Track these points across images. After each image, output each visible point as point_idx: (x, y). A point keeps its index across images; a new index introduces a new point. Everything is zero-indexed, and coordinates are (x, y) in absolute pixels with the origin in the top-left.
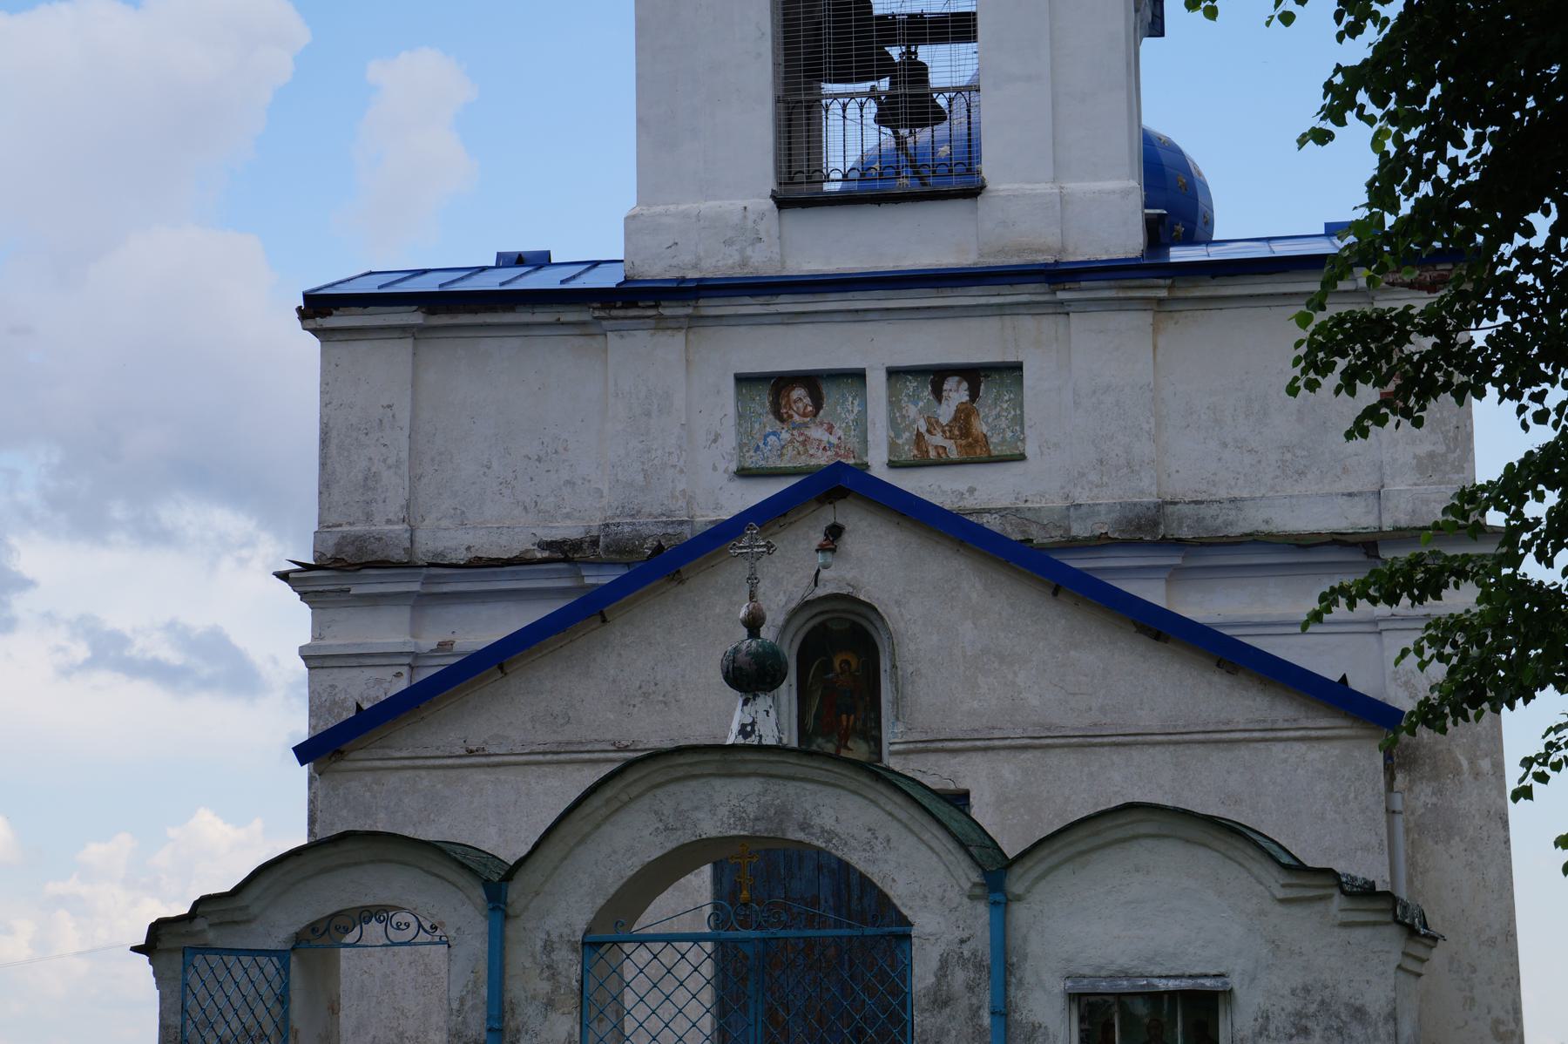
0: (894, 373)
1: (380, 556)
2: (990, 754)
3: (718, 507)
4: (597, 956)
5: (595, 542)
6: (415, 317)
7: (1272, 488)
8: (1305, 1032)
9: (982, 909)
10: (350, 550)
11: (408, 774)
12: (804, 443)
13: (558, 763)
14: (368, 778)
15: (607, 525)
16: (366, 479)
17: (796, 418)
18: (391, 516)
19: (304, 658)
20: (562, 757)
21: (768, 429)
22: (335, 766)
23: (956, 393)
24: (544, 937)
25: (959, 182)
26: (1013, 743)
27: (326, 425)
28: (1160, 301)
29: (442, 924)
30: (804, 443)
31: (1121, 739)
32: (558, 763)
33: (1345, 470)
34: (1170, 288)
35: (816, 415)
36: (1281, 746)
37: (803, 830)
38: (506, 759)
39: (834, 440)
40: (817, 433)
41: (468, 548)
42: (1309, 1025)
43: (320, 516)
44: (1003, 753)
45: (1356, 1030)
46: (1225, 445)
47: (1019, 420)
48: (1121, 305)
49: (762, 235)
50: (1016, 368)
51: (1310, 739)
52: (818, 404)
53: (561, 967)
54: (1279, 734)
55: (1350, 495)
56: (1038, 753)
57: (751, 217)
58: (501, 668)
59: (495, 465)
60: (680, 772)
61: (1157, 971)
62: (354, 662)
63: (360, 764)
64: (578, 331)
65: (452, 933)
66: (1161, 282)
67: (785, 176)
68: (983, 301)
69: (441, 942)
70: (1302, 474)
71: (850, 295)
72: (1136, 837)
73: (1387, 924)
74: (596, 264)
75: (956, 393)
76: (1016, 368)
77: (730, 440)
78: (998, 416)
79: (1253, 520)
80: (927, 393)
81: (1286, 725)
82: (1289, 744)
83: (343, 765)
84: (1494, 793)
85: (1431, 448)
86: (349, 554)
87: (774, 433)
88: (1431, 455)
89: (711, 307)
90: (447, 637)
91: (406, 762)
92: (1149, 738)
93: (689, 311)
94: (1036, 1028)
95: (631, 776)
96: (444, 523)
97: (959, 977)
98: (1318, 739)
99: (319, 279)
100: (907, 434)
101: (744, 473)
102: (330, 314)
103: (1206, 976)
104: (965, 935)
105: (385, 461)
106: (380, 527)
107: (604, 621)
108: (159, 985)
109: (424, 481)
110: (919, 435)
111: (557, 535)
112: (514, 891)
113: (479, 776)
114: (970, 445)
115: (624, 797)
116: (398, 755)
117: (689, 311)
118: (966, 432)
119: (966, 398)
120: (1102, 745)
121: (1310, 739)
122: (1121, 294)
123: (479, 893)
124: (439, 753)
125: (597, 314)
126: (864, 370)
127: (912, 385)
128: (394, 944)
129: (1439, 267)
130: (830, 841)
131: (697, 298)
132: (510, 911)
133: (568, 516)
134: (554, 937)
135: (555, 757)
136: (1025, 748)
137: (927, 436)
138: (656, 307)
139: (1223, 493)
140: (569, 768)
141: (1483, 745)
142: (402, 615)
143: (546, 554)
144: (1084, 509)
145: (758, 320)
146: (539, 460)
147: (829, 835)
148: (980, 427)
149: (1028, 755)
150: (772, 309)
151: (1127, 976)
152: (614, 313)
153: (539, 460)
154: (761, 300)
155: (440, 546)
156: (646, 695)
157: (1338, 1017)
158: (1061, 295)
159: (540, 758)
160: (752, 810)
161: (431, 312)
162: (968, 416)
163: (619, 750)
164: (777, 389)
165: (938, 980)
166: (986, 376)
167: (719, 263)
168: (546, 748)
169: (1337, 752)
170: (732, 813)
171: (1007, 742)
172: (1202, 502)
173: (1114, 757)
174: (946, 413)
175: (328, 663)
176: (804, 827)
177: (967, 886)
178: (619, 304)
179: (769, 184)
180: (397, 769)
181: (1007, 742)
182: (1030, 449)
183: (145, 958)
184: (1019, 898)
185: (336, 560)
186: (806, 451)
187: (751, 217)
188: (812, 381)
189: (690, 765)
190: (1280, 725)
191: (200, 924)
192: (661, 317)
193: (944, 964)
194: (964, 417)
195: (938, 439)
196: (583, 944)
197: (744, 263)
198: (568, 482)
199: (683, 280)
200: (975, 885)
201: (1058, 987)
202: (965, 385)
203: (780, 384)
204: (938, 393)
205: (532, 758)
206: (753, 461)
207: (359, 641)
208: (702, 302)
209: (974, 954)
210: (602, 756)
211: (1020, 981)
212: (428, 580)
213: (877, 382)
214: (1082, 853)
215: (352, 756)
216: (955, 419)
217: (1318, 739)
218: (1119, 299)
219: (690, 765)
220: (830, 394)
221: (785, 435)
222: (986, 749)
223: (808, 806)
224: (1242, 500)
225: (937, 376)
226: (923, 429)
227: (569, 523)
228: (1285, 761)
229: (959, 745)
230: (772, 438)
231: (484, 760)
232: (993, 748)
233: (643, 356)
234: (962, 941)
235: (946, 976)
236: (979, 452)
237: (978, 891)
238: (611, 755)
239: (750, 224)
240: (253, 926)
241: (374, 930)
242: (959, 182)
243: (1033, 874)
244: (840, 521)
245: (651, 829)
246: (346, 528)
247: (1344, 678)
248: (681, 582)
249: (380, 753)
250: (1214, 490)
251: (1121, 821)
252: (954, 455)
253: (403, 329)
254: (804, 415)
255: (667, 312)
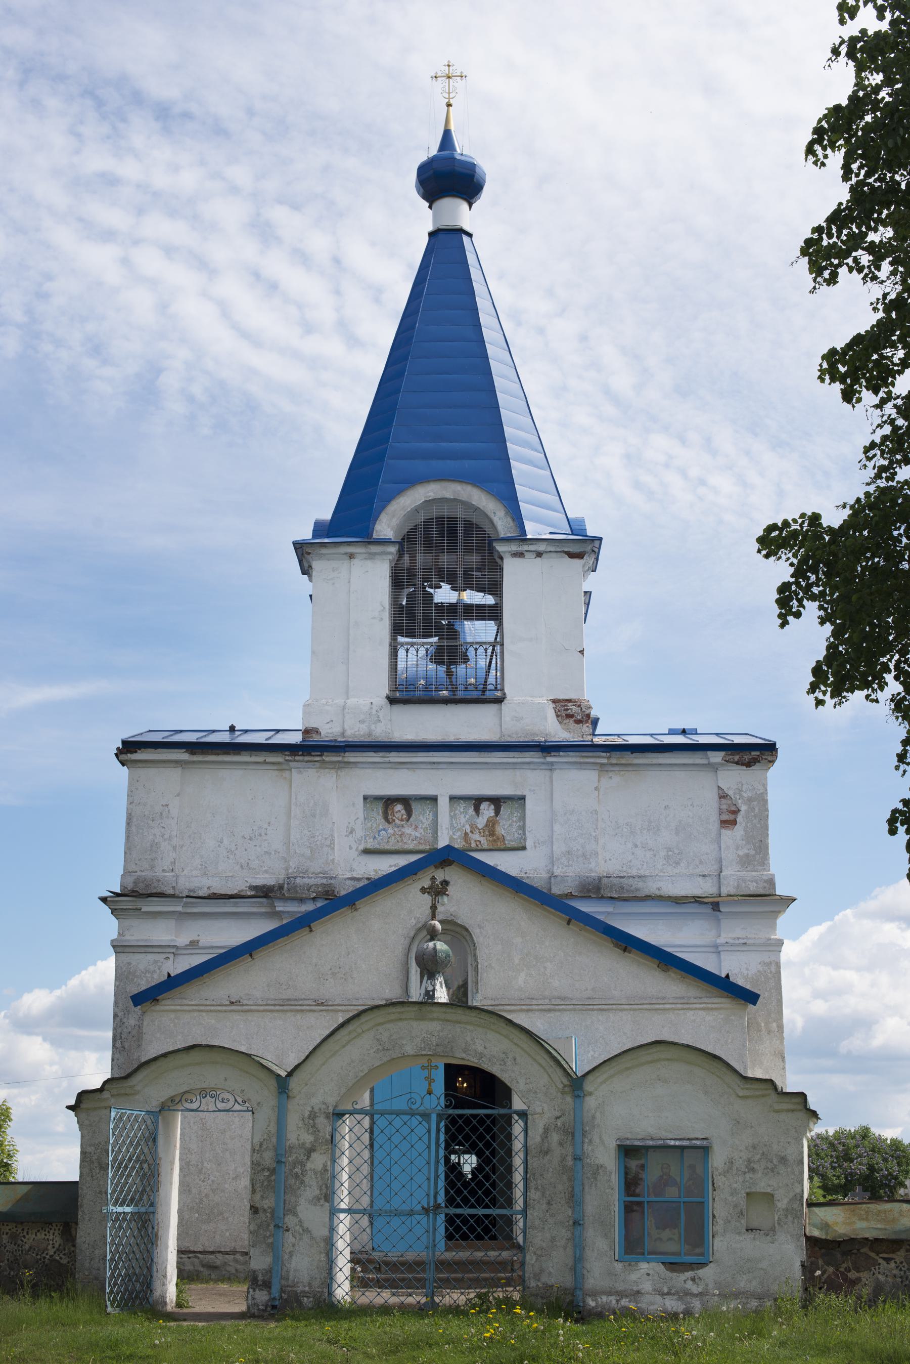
0: (452, 799)
1: (159, 891)
2: (530, 1013)
3: (352, 870)
4: (341, 1121)
5: (281, 887)
6: (183, 755)
7: (662, 871)
8: (753, 1170)
9: (569, 1099)
10: (141, 885)
11: (196, 1014)
12: (401, 836)
13: (282, 1011)
14: (172, 1016)
15: (289, 878)
16: (152, 846)
17: (397, 821)
18: (165, 868)
19: (114, 947)
20: (285, 1008)
21: (381, 827)
22: (153, 1008)
23: (487, 811)
24: (310, 1109)
25: (488, 696)
26: (543, 1007)
27: (130, 814)
28: (602, 765)
29: (249, 1100)
30: (401, 836)
31: (604, 1007)
32: (282, 1011)
33: (701, 862)
34: (609, 758)
35: (408, 820)
36: (692, 1012)
37: (465, 1052)
38: (253, 1008)
39: (418, 834)
40: (408, 830)
41: (209, 888)
42: (755, 1166)
43: (124, 866)
44: (537, 1013)
45: (782, 1169)
46: (636, 846)
47: (523, 828)
48: (581, 765)
49: (381, 718)
50: (523, 798)
51: (708, 1009)
52: (409, 813)
53: (320, 1126)
54: (691, 1006)
55: (704, 876)
56: (558, 1013)
57: (375, 708)
58: (251, 955)
59: (225, 841)
60: (393, 1017)
61: (671, 1136)
62: (143, 950)
63: (168, 1008)
64: (275, 768)
65: (255, 1106)
66: (604, 754)
67: (393, 687)
68: (520, 760)
69: (249, 1111)
70: (678, 863)
71: (431, 754)
72: (659, 1060)
73: (800, 1110)
74: (214, 731)
75: (487, 811)
76: (523, 798)
77: (359, 833)
78: (511, 825)
79: (651, 888)
80: (471, 811)
81: (695, 1001)
82: (696, 1012)
83: (158, 1008)
84: (778, 1042)
85: (747, 852)
86: (141, 888)
87: (384, 830)
88: (747, 855)
89: (351, 757)
90: (196, 938)
91: (195, 1008)
92: (620, 1007)
93: (340, 759)
94: (599, 1167)
95: (363, 1018)
96: (194, 873)
97: (555, 1137)
98: (712, 1009)
99: (130, 732)
100: (459, 833)
101: (367, 852)
102: (136, 752)
103: (697, 1139)
104: (559, 1114)
105: (163, 836)
106: (159, 873)
107: (311, 931)
108: (81, 1129)
109: (184, 848)
110: (466, 834)
111: (259, 882)
112: (293, 1083)
113: (236, 1017)
114: (495, 841)
115: (360, 1031)
116: (190, 1003)
117: (340, 759)
118: (492, 833)
119: (493, 814)
120: (593, 1010)
121: (708, 1009)
122: (582, 760)
123: (273, 1083)
124: (214, 1003)
125: (287, 758)
126: (437, 796)
127: (462, 806)
128: (220, 1111)
129: (753, 753)
130: (480, 1059)
131: (345, 752)
132: (290, 1094)
133: (266, 872)
134: (316, 1109)
135: (281, 1008)
136: (550, 1010)
137: (470, 834)
138: (321, 755)
139: (634, 872)
140: (289, 1014)
141: (773, 1015)
142: (171, 923)
143: (253, 893)
144: (559, 879)
145: (379, 765)
146: (251, 839)
147: (481, 1056)
148: (500, 830)
149: (552, 1014)
150: (387, 760)
151: (652, 1139)
152: (297, 758)
153: (251, 839)
154: (381, 754)
155: (192, 886)
156: (334, 974)
157: (771, 1162)
158: (549, 759)
159: (272, 1008)
160: (434, 1040)
161: (193, 753)
162: (494, 825)
163: (318, 1005)
164: (387, 804)
165: (543, 1140)
166: (504, 802)
167: (355, 731)
168: (276, 1002)
169: (722, 1016)
170: (423, 1040)
171: (540, 1007)
172: (623, 877)
173: (600, 1017)
174: (481, 822)
175: (127, 950)
176: (465, 1051)
177: (561, 1086)
178: (300, 753)
179: (386, 691)
180: (189, 1011)
181: (540, 1007)
182: (529, 844)
183: (72, 1113)
184: (590, 1094)
185: (133, 891)
186: (402, 840)
187: (375, 708)
188: (406, 801)
189: (400, 1013)
190: (692, 1000)
191: (106, 1095)
192: (323, 762)
193: (546, 1131)
194: (491, 825)
195: (476, 836)
196: (334, 1114)
197: (370, 735)
198: (266, 853)
199: (336, 741)
200: (565, 1086)
201: (613, 1144)
202: (492, 807)
203: (389, 802)
204: (477, 810)
205: (267, 1007)
206: (371, 844)
207: (145, 938)
208: (347, 754)
209: (564, 1125)
210: (308, 1008)
211: (590, 1141)
212: (186, 905)
213: (443, 803)
214: (627, 1069)
215: (163, 1002)
216: (486, 826)
217: (712, 1009)
218: (581, 763)
219: (400, 1013)
220: (416, 807)
221: (390, 831)
222: (528, 1011)
223: (468, 1039)
224: (645, 877)
225: (477, 801)
226: (468, 831)
227: (267, 876)
228: (694, 1021)
229: (513, 1008)
230: (383, 832)
231: (239, 1008)
232: (532, 1010)
233: (313, 782)
234: (557, 1118)
235: (547, 1137)
236: (500, 845)
237: (567, 1089)
238: (313, 1008)
239: (374, 712)
240: (137, 1097)
241: (208, 1103)
242: (488, 696)
243: (599, 1080)
244: (447, 879)
245: (375, 1049)
246: (139, 873)
247: (727, 976)
248: (356, 910)
249: (179, 1002)
250: (630, 871)
251: (651, 1051)
252: (486, 846)
253: (177, 762)
254: (402, 820)
255: (327, 759)
